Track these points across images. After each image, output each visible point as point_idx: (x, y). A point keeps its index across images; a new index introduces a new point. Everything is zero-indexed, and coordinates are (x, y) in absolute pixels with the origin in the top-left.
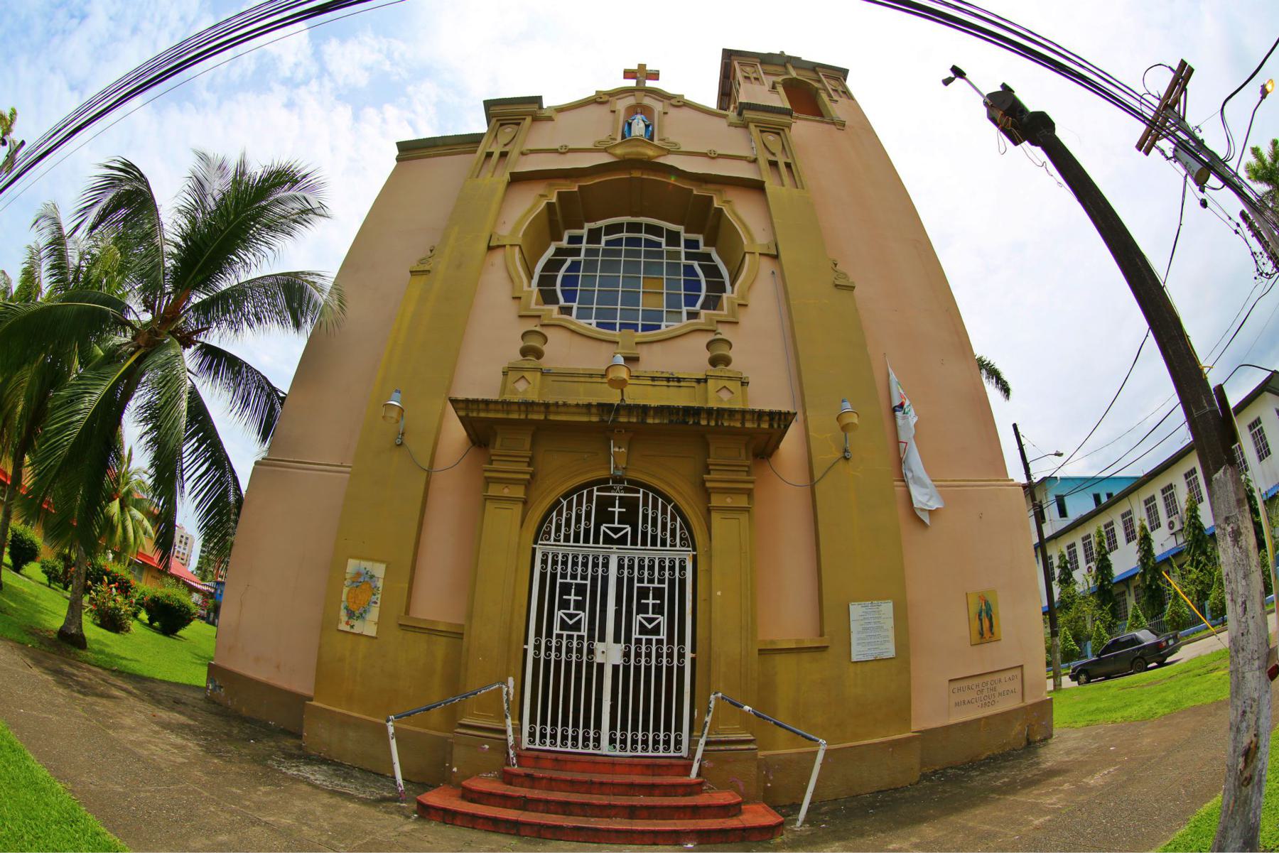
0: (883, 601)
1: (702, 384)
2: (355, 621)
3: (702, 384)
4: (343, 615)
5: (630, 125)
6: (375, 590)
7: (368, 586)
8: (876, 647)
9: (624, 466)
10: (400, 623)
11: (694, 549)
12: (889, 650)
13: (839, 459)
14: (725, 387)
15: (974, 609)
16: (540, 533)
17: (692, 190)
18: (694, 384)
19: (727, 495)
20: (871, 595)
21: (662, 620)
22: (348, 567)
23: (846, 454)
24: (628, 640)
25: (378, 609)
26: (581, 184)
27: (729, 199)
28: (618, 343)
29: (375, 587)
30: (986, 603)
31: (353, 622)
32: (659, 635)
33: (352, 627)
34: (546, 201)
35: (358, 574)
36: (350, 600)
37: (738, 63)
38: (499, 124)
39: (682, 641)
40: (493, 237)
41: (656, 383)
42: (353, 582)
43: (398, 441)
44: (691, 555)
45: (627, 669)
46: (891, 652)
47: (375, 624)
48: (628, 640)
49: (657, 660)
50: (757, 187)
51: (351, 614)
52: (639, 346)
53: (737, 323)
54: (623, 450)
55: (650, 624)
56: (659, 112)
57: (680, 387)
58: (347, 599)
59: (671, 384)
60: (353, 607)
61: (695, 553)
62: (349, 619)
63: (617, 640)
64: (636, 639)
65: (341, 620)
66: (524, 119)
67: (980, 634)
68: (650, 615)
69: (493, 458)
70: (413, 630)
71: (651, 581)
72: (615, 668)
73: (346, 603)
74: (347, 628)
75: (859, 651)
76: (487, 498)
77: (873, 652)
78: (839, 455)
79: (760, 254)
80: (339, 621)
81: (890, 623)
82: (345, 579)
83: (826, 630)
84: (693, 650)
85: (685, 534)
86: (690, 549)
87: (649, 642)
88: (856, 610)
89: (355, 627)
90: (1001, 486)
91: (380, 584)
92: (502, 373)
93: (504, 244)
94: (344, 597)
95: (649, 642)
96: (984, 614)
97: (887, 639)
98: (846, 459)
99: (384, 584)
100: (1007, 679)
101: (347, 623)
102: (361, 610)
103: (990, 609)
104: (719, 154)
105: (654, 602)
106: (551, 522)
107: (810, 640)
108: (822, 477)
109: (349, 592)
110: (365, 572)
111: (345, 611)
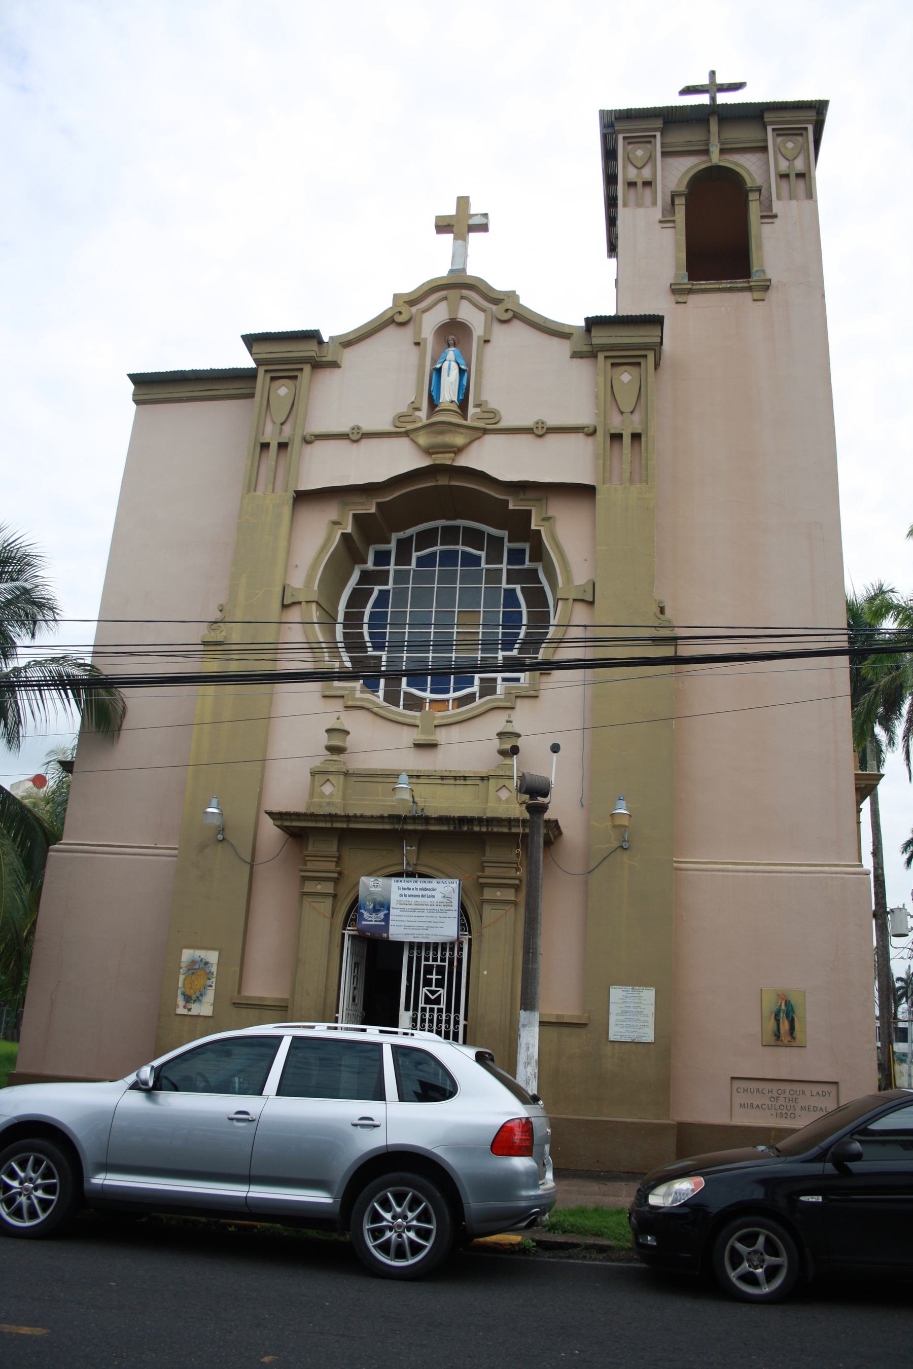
0: (645, 988)
1: (485, 782)
4: (181, 1001)
5: (439, 371)
6: (210, 974)
8: (635, 1030)
9: (415, 863)
10: (234, 1001)
11: (470, 933)
13: (618, 847)
14: (504, 786)
18: (478, 782)
19: (496, 889)
20: (634, 980)
21: (443, 992)
22: (183, 956)
24: (416, 1008)
25: (214, 991)
27: (550, 514)
28: (418, 726)
29: (210, 972)
30: (788, 1003)
31: (189, 1006)
32: (440, 1004)
33: (189, 1010)
34: (340, 532)
35: (193, 962)
36: (186, 986)
38: (269, 376)
39: (457, 1010)
40: (286, 588)
41: (445, 782)
42: (189, 970)
43: (220, 837)
44: (467, 938)
46: (648, 1035)
47: (211, 1005)
48: (416, 1008)
49: (437, 1026)
51: (188, 999)
52: (438, 729)
53: (537, 697)
54: (414, 848)
55: (433, 995)
56: (479, 337)
57: (466, 785)
58: (184, 985)
59: (458, 782)
60: (188, 992)
61: (470, 937)
62: (186, 1003)
63: (407, 1009)
64: (422, 1008)
65: (178, 1005)
66: (301, 370)
67: (776, 1035)
68: (433, 988)
69: (307, 858)
70: (245, 1006)
71: (435, 960)
73: (183, 989)
74: (185, 1012)
76: (304, 894)
77: (630, 1034)
79: (574, 600)
80: (176, 1006)
82: (181, 968)
84: (466, 1019)
85: (464, 920)
87: (432, 1010)
88: (617, 994)
89: (192, 1010)
90: (836, 873)
92: (310, 774)
93: (300, 601)
94: (180, 985)
95: (432, 1010)
97: (646, 1024)
99: (217, 969)
100: (814, 1093)
101: (185, 1007)
102: (198, 994)
103: (793, 1010)
104: (548, 429)
105: (437, 977)
109: (185, 979)
110: (200, 959)
111: (183, 996)
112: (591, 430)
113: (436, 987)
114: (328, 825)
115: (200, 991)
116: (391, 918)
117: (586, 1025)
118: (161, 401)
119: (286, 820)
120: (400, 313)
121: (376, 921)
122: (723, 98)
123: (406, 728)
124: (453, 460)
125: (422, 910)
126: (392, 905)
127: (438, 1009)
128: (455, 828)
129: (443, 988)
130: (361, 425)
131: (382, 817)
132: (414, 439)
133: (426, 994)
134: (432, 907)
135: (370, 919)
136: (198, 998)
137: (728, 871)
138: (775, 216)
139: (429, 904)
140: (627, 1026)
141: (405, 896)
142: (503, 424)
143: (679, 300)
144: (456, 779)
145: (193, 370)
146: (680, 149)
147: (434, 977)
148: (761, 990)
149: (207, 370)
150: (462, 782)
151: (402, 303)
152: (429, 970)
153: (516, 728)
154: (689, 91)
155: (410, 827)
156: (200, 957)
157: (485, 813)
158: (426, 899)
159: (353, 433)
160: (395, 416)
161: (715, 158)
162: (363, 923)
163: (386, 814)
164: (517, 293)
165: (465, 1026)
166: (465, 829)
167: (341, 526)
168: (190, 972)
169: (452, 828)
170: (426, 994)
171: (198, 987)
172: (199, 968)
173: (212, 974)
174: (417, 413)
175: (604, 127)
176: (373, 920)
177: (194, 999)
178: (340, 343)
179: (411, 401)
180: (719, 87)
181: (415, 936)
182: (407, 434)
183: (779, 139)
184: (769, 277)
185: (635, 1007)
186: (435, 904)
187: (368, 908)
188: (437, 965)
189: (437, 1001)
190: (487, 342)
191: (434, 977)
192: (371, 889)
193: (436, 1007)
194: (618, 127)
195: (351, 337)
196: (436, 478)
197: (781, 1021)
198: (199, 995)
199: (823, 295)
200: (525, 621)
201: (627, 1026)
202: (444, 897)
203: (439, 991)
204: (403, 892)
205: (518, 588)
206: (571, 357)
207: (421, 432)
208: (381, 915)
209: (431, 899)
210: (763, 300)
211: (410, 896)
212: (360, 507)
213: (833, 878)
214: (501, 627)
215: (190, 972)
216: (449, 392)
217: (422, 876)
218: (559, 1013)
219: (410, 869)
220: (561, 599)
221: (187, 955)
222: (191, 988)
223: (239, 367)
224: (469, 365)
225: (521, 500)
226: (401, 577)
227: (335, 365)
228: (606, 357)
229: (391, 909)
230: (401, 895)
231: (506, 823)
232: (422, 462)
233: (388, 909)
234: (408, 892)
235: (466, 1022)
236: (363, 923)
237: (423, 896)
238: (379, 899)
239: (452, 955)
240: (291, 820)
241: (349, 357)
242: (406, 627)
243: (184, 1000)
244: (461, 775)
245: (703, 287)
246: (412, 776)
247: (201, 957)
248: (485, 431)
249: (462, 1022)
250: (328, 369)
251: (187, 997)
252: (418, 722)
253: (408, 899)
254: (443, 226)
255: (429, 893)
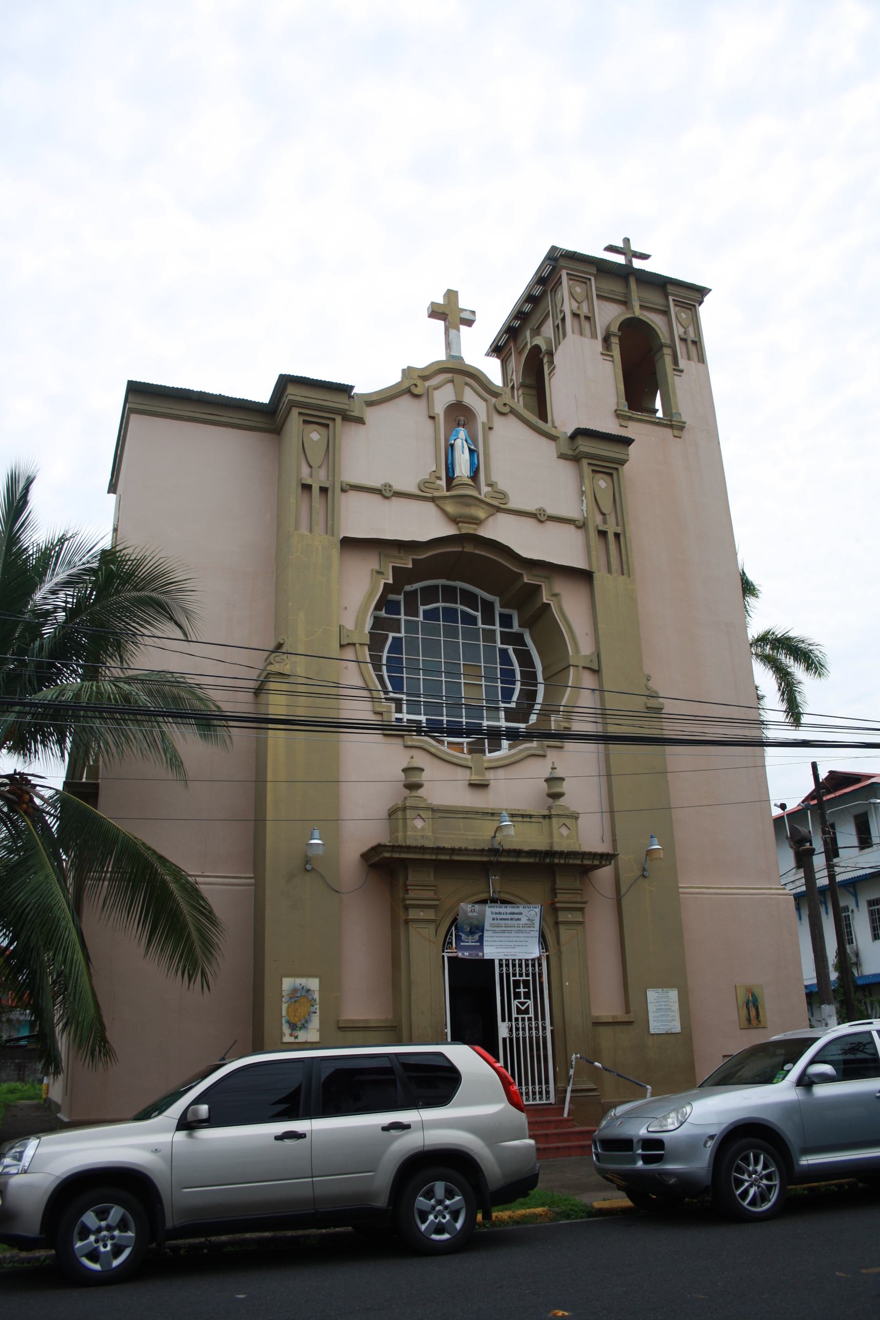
1: (547, 820)
2: (299, 1032)
3: (547, 820)
4: (286, 1030)
5: (452, 446)
6: (313, 1001)
7: (305, 999)
12: (676, 1027)
15: (742, 999)
16: (447, 944)
17: (521, 575)
18: (541, 820)
19: (568, 912)
20: (663, 984)
21: (530, 1003)
23: (645, 873)
24: (510, 1020)
25: (318, 1017)
26: (415, 557)
29: (313, 999)
30: (753, 995)
31: (296, 1033)
32: (529, 1014)
33: (296, 1037)
35: (295, 990)
36: (290, 1014)
37: (568, 274)
39: (543, 1018)
42: (291, 998)
45: (511, 1039)
46: (676, 1027)
47: (317, 1031)
48: (510, 1020)
50: (584, 576)
51: (293, 1027)
56: (483, 423)
58: (288, 1013)
59: (525, 820)
60: (292, 1020)
61: (547, 954)
63: (503, 1020)
64: (515, 1018)
65: (284, 1033)
68: (522, 1000)
71: (521, 975)
72: (504, 1039)
73: (287, 1017)
74: (292, 1040)
75: (656, 1026)
78: (639, 873)
79: (584, 668)
80: (282, 1034)
81: (676, 1007)
82: (283, 997)
83: (632, 1009)
84: (552, 1025)
86: (544, 951)
87: (523, 1019)
88: (652, 995)
91: (316, 996)
95: (523, 1019)
96: (751, 1004)
98: (644, 876)
101: (291, 1035)
102: (303, 1021)
104: (549, 517)
106: (451, 935)
107: (621, 1016)
108: (627, 891)
109: (288, 1008)
110: (301, 987)
111: (288, 1025)
112: (581, 524)
113: (524, 999)
114: (434, 857)
115: (304, 1018)
116: (485, 939)
117: (632, 1022)
118: (223, 424)
119: (396, 852)
120: (416, 385)
121: (472, 942)
122: (637, 264)
123: (460, 769)
124: (475, 530)
125: (510, 932)
126: (486, 928)
127: (528, 1018)
128: (540, 860)
129: (530, 999)
130: (392, 484)
131: (483, 850)
132: (440, 505)
133: (517, 1006)
134: (518, 929)
135: (467, 941)
136: (303, 1025)
137: (764, 894)
138: (682, 371)
139: (516, 926)
140: (662, 1021)
141: (497, 919)
142: (511, 505)
143: (623, 424)
144: (523, 817)
145: (201, 391)
146: (606, 295)
147: (522, 990)
148: (735, 986)
149: (216, 395)
150: (528, 820)
151: (417, 377)
152: (517, 984)
153: (559, 773)
154: (611, 249)
155: (504, 859)
156: (300, 984)
157: (551, 847)
158: (513, 922)
159: (385, 490)
160: (421, 481)
161: (638, 312)
162: (462, 944)
163: (486, 848)
164: (405, 367)
165: (552, 1031)
166: (548, 861)
167: (383, 576)
168: (293, 1000)
169: (537, 860)
170: (517, 1006)
171: (302, 1015)
172: (301, 996)
173: (315, 1001)
174: (438, 482)
175: (549, 259)
176: (470, 941)
177: (299, 1026)
178: (365, 402)
179: (433, 470)
180: (633, 253)
181: (506, 954)
182: (433, 499)
183: (571, 282)
184: (684, 420)
185: (665, 1005)
186: (521, 926)
187: (465, 931)
188: (523, 980)
189: (526, 1011)
190: (491, 428)
191: (522, 990)
192: (469, 914)
193: (526, 1016)
194: (562, 262)
195: (374, 398)
196: (462, 544)
197: (750, 1009)
198: (304, 1022)
199: (719, 443)
200: (518, 677)
201: (662, 1021)
202: (528, 920)
203: (527, 1002)
204: (495, 916)
205: (510, 649)
206: (365, 424)
207: (448, 501)
208: (477, 937)
209: (518, 922)
210: (680, 438)
211: (501, 919)
212: (398, 561)
213: (771, 898)
214: (499, 680)
215: (293, 1000)
216: (463, 469)
217: (504, 902)
218: (614, 1014)
219: (496, 896)
220: (573, 666)
221: (288, 983)
222: (295, 1015)
223: (207, 392)
224: (476, 445)
225: (535, 576)
226: (411, 627)
227: (360, 421)
228: (300, 413)
229: (485, 931)
230: (494, 919)
231: (599, 857)
232: (448, 530)
233: (483, 931)
234: (499, 916)
235: (552, 1028)
236: (462, 944)
237: (512, 919)
238: (475, 922)
239: (534, 970)
240: (400, 852)
241: (371, 415)
242: (442, 675)
243: (290, 1028)
244: (528, 813)
245: (639, 417)
246: (488, 813)
247: (302, 985)
248: (499, 510)
249: (549, 1028)
250: (353, 423)
251: (292, 1025)
252: (470, 764)
253: (499, 922)
254: (436, 312)
255: (516, 916)
